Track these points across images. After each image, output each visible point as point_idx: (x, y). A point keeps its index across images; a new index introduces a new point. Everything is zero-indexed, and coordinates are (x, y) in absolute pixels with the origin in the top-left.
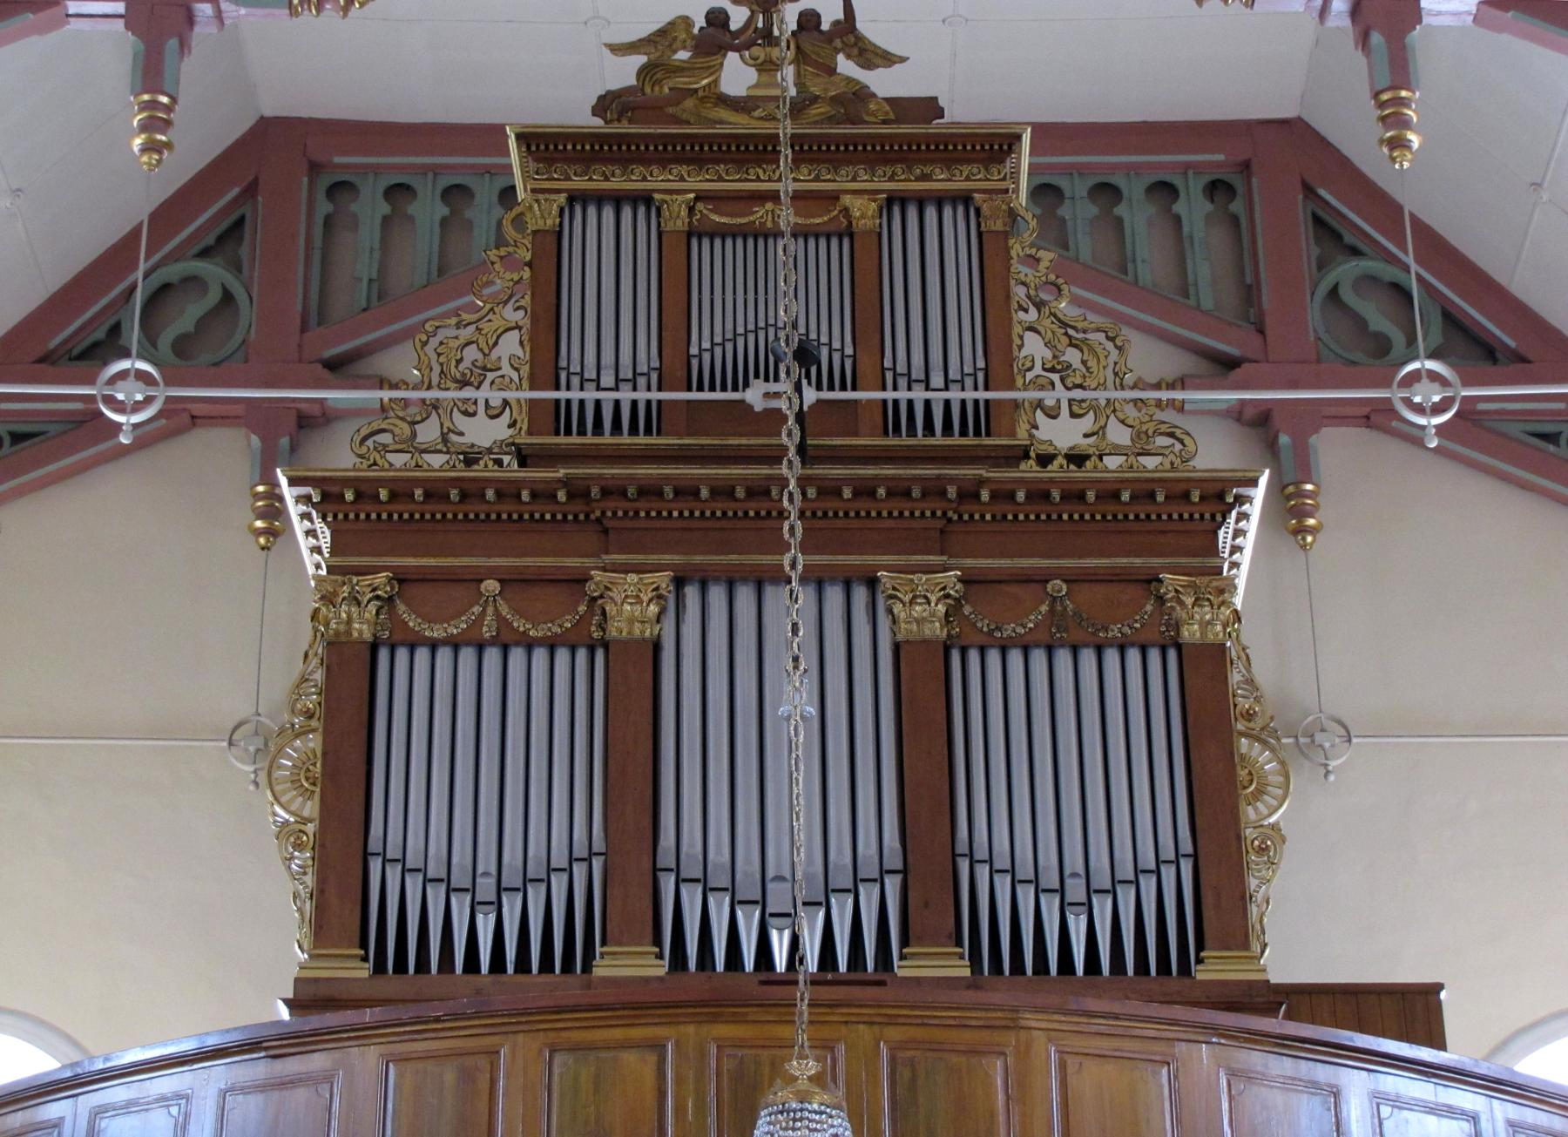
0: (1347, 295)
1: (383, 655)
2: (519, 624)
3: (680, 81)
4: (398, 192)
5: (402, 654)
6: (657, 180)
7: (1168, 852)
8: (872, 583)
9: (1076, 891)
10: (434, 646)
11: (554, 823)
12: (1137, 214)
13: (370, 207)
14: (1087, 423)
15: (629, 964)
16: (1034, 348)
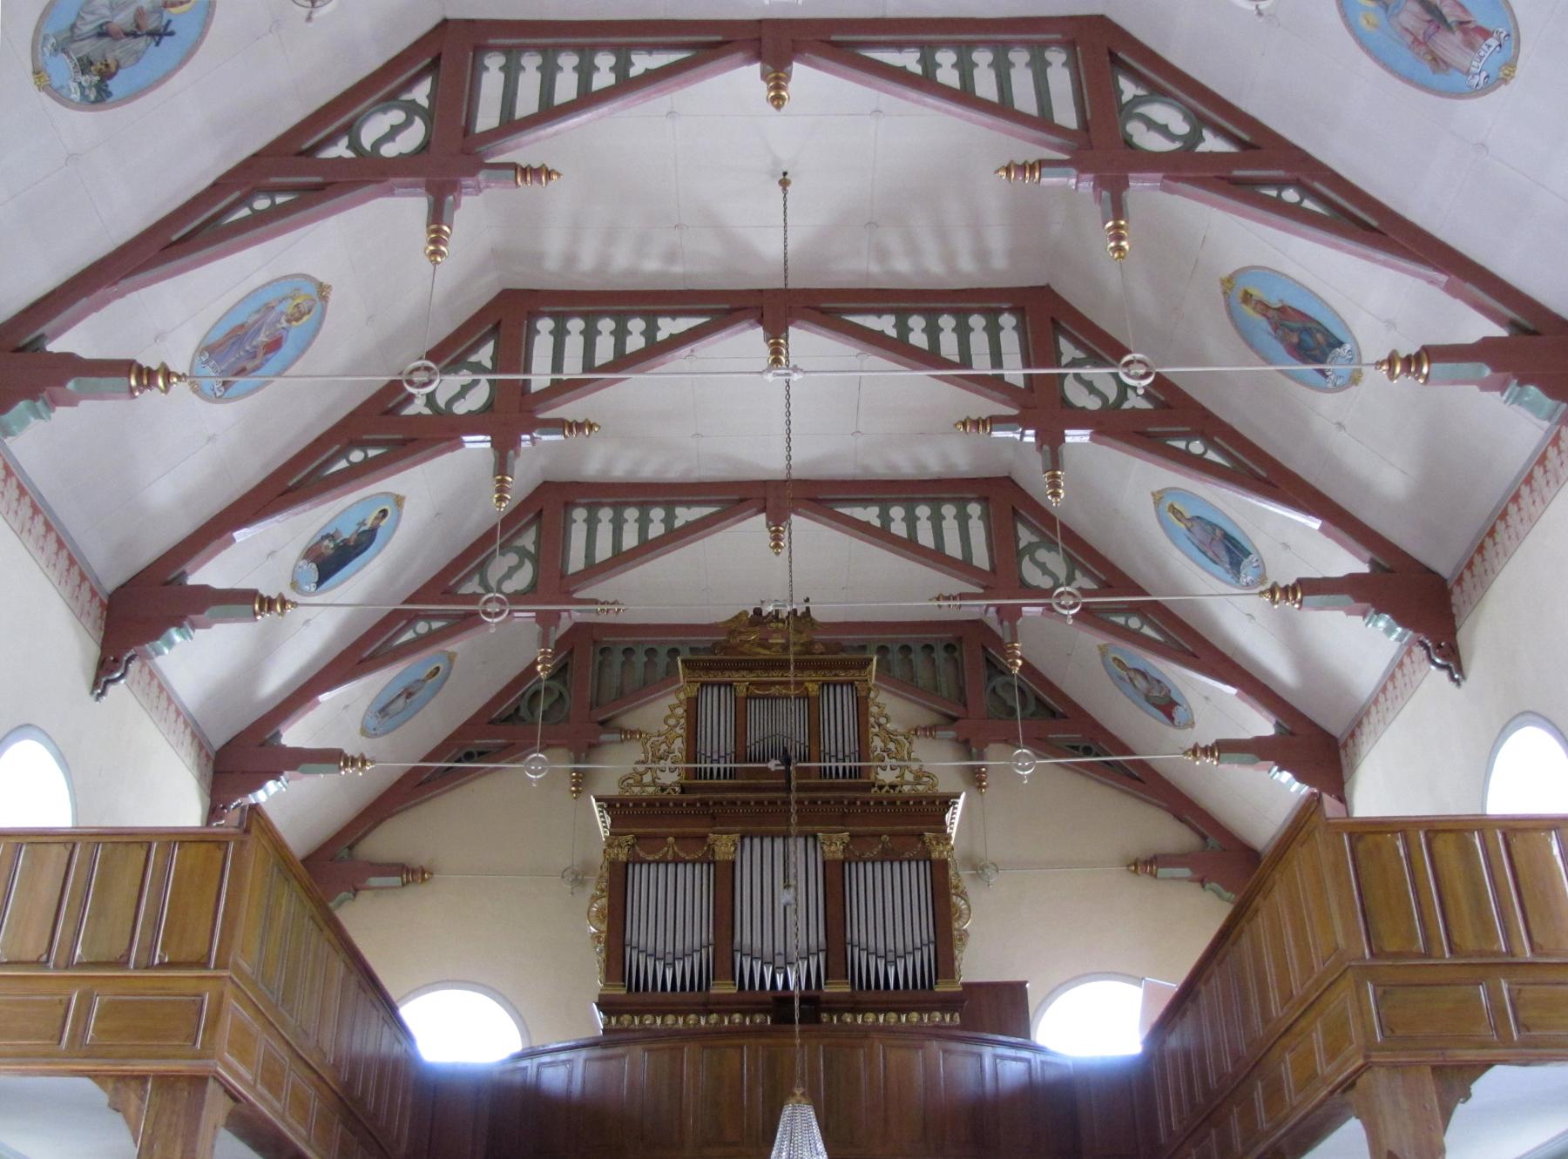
0: (1000, 691)
2: (682, 854)
4: (628, 652)
5: (637, 867)
6: (735, 677)
8: (815, 837)
9: (891, 957)
11: (696, 932)
12: (918, 658)
13: (617, 658)
14: (897, 772)
16: (877, 743)
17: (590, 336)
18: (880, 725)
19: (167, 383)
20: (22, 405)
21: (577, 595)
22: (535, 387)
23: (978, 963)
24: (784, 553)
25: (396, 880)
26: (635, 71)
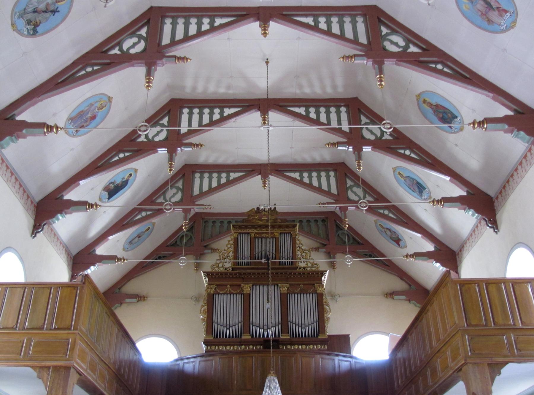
0: (340, 235)
2: (232, 291)
4: (214, 222)
5: (217, 295)
6: (250, 231)
8: (278, 285)
9: (303, 326)
11: (237, 318)
12: (313, 224)
13: (210, 224)
14: (306, 263)
16: (299, 253)
17: (201, 114)
18: (300, 247)
19: (57, 131)
20: (8, 138)
21: (196, 203)
22: (182, 132)
23: (333, 328)
24: (267, 188)
25: (135, 300)
26: (216, 24)
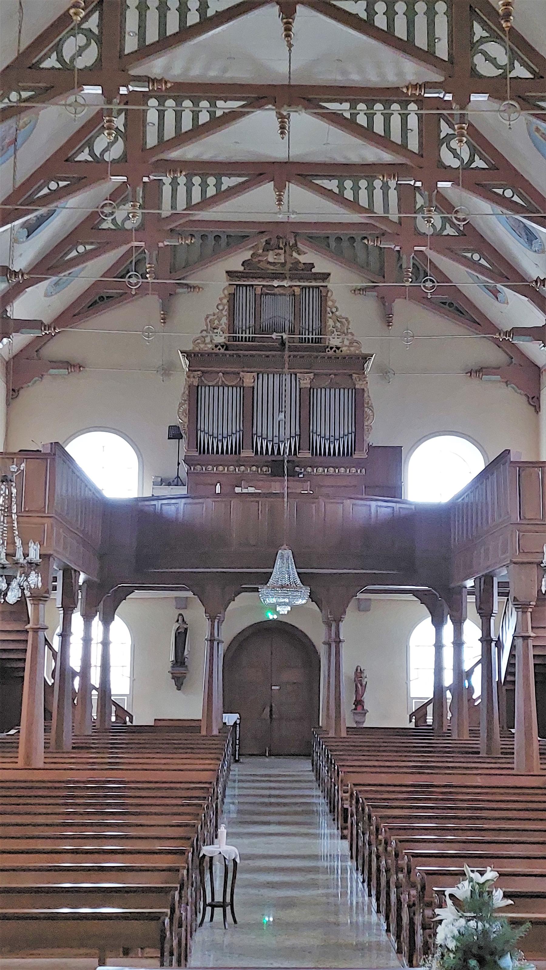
1: (200, 388)
2: (226, 383)
3: (260, 258)
7: (350, 432)
9: (332, 439)
10: (209, 386)
15: (247, 453)
16: (330, 322)
17: (189, 186)
18: (332, 313)
21: (133, 72)
22: (163, 216)
23: (377, 436)
24: (286, 137)
26: (224, 187)
